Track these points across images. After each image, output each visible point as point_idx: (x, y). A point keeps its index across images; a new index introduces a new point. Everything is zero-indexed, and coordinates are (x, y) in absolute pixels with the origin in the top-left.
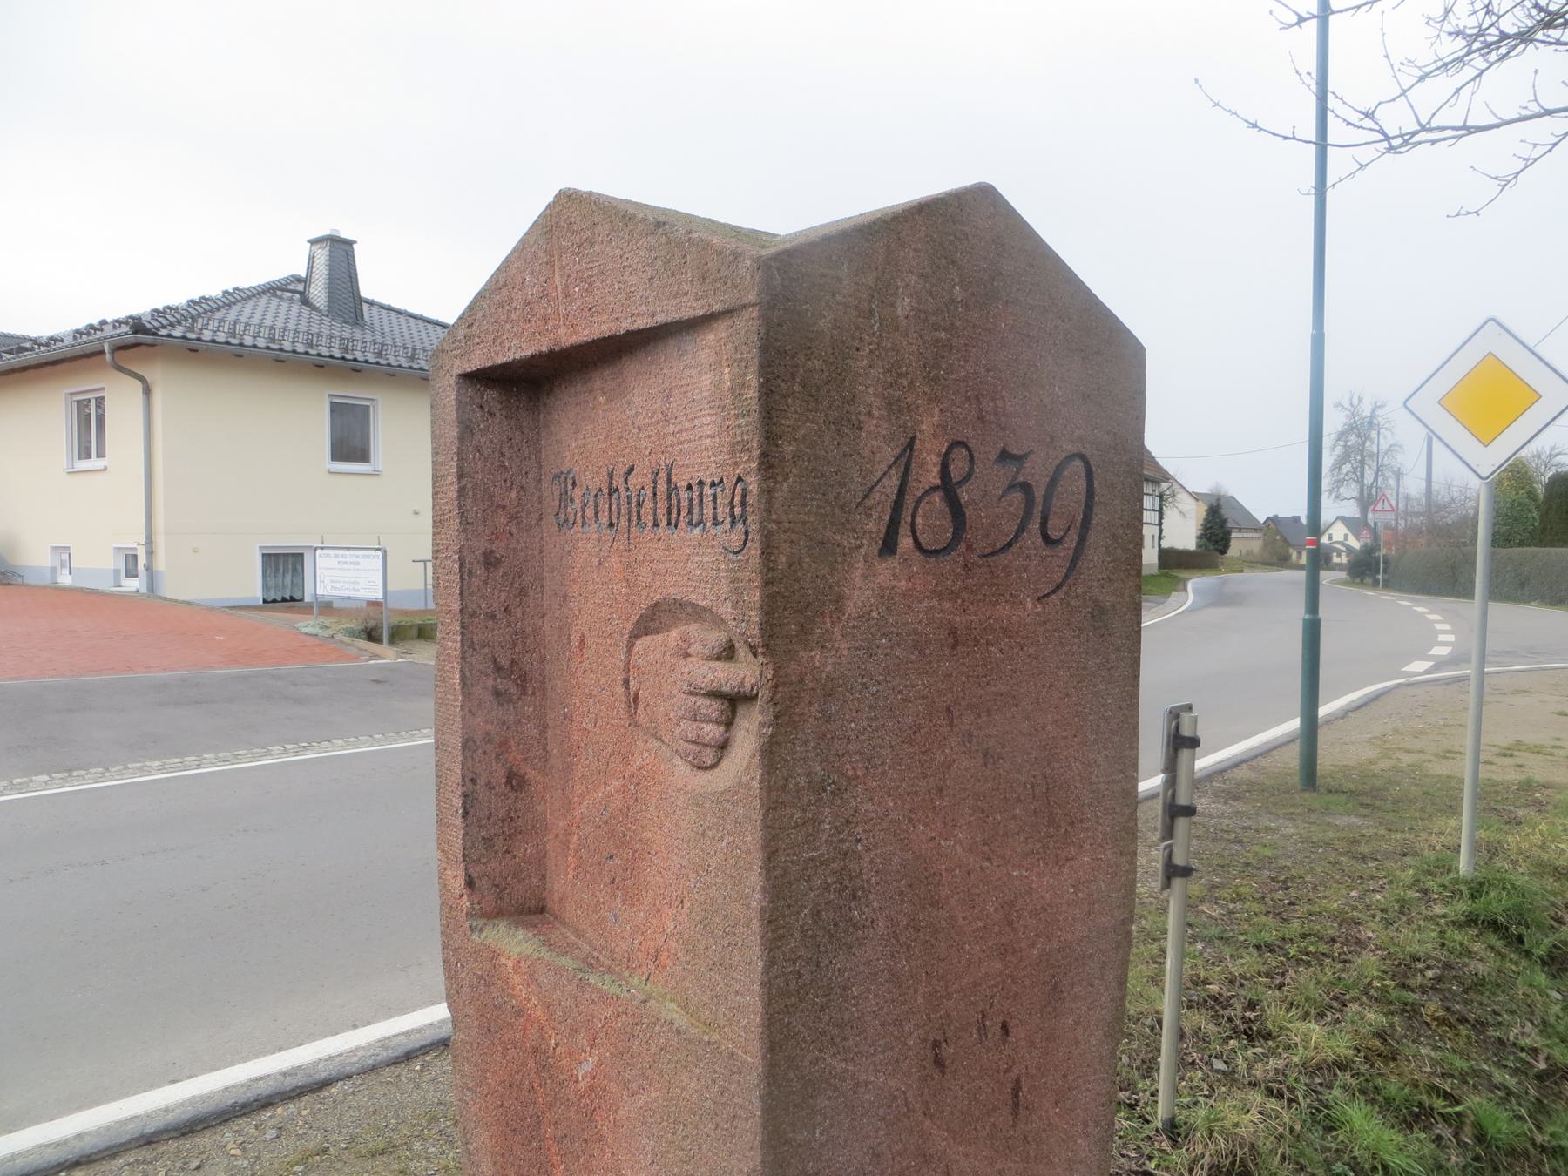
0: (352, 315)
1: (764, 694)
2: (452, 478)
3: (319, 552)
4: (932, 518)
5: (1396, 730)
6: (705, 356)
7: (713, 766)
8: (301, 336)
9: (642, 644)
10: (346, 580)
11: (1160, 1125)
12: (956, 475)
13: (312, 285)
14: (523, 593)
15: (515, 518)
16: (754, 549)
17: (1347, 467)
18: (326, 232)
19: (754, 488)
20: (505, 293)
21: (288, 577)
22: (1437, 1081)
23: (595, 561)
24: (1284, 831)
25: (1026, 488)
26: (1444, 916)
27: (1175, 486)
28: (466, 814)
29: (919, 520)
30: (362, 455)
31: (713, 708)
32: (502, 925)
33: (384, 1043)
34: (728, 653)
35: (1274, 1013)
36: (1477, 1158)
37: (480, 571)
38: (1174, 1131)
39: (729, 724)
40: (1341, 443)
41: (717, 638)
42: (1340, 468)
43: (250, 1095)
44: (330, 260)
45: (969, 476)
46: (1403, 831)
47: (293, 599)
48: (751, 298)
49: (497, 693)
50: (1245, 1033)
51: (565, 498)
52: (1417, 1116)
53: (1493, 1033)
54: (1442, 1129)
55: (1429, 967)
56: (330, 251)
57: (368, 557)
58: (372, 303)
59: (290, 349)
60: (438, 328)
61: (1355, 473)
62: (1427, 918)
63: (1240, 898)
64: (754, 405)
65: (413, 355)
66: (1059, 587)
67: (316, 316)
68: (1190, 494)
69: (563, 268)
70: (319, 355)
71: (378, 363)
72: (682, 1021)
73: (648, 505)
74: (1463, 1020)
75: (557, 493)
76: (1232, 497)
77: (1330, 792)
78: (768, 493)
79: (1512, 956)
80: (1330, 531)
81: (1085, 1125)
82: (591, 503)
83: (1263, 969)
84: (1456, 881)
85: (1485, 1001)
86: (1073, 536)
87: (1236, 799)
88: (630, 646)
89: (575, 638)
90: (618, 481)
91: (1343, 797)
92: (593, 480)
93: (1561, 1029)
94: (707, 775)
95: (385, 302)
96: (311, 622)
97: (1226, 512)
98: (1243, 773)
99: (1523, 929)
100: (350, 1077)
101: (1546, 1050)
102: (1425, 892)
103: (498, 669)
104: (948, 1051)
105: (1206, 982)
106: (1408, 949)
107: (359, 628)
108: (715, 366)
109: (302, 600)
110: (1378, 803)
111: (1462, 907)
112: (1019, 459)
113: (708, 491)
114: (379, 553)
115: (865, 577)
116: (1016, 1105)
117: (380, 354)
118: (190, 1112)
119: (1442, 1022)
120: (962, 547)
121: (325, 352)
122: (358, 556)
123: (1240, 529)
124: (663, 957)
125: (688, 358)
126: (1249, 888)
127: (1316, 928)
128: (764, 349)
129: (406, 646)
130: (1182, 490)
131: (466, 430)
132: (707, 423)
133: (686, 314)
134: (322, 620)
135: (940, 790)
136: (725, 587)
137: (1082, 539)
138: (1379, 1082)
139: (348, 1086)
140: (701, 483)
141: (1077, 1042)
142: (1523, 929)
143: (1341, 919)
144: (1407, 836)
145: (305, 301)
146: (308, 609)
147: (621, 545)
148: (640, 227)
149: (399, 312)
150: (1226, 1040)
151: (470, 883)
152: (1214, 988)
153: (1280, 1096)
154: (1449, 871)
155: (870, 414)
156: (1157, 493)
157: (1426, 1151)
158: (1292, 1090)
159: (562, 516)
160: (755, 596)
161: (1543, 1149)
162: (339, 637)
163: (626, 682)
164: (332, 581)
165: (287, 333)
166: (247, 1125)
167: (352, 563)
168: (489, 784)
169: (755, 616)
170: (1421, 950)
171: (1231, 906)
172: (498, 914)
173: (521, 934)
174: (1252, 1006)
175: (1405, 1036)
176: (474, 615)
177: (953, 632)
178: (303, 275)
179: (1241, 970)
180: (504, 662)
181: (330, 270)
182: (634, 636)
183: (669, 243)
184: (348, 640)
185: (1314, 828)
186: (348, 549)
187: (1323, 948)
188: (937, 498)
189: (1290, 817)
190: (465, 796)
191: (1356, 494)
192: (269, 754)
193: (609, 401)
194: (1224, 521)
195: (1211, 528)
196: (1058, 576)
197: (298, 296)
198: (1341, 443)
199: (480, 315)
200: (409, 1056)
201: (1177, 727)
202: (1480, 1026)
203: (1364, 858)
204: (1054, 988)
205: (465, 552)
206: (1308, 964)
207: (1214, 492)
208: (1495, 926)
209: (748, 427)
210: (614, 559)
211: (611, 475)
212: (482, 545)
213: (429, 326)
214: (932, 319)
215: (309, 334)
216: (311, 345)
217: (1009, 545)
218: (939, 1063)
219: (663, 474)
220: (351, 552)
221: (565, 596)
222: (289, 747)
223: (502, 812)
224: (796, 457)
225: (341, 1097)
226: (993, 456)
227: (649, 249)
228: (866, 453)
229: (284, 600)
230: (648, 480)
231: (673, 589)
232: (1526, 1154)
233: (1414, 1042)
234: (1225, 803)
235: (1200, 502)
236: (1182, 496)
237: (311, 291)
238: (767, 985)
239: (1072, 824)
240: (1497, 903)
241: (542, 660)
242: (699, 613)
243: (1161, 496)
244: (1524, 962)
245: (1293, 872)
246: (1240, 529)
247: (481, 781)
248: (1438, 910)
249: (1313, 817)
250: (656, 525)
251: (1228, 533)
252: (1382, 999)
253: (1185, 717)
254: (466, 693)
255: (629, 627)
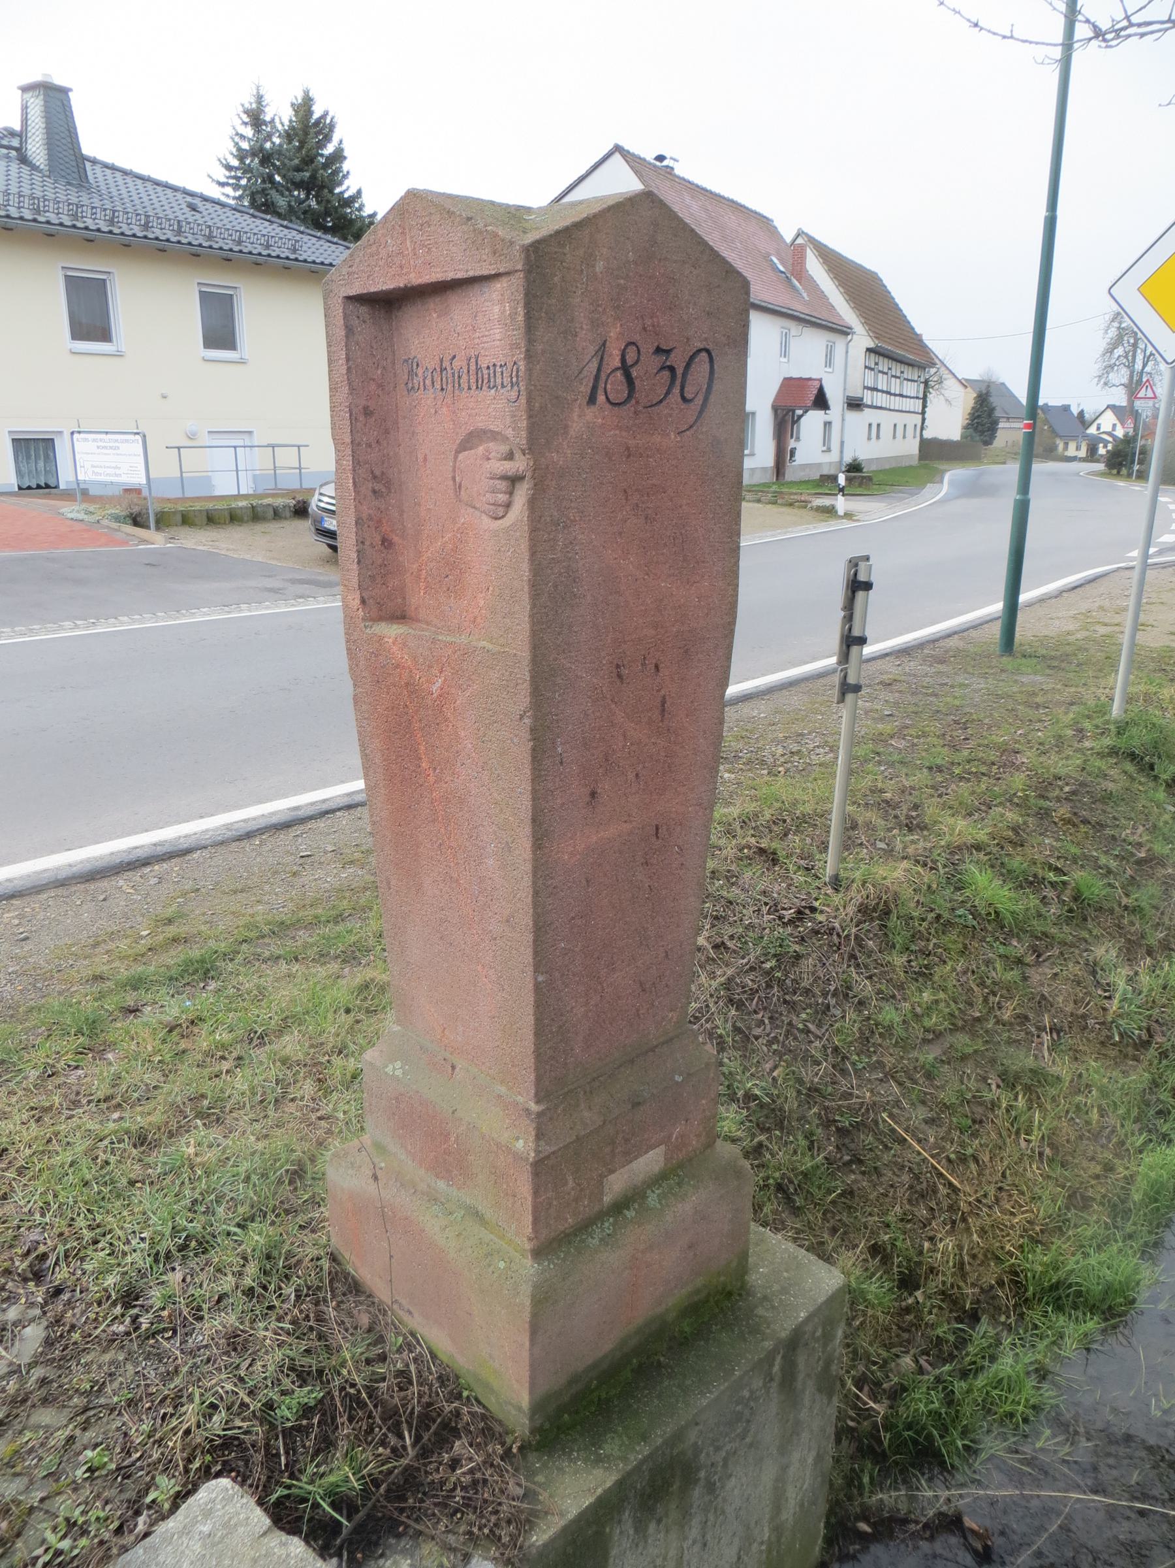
0: (76, 176)
1: (529, 474)
2: (342, 361)
3: (76, 436)
4: (616, 385)
5: (1101, 608)
6: (495, 296)
7: (503, 517)
8: (27, 201)
9: (461, 456)
10: (107, 464)
11: (827, 880)
12: (629, 362)
13: (29, 141)
14: (387, 432)
15: (381, 386)
16: (523, 399)
17: (1119, 351)
18: (37, 77)
19: (522, 368)
20: (374, 248)
21: (41, 464)
22: (1052, 861)
23: (433, 411)
24: (975, 686)
25: (672, 369)
26: (1092, 749)
27: (943, 370)
28: (359, 562)
29: (609, 386)
30: (104, 334)
31: (503, 485)
32: (383, 624)
33: (228, 827)
34: (510, 456)
35: (931, 810)
36: (1070, 911)
37: (362, 418)
38: (837, 883)
39: (511, 493)
40: (1116, 324)
41: (504, 449)
42: (1111, 352)
43: (132, 857)
44: (46, 111)
45: (637, 362)
46: (1077, 686)
47: (47, 486)
48: (520, 267)
49: (374, 492)
50: (907, 825)
51: (412, 374)
52: (1031, 883)
53: (1108, 831)
54: (1050, 893)
55: (1067, 784)
56: (46, 102)
57: (127, 441)
58: (94, 162)
59: (16, 215)
60: (169, 191)
61: (1126, 357)
62: (1077, 750)
63: (925, 735)
64: (522, 324)
65: (147, 223)
66: (691, 427)
67: (37, 177)
68: (960, 381)
69: (412, 237)
70: (48, 222)
71: (110, 232)
72: (489, 646)
73: (465, 377)
74: (1085, 822)
75: (406, 371)
76: (1003, 384)
77: (1025, 656)
78: (529, 370)
79: (1142, 780)
80: (1098, 421)
81: (705, 732)
82: (429, 377)
83: (930, 783)
84: (1107, 722)
85: (1109, 810)
86: (701, 397)
87: (942, 662)
88: (456, 458)
89: (420, 458)
90: (446, 364)
91: (1035, 660)
92: (431, 363)
93: (1166, 830)
94: (500, 522)
95: (108, 160)
96: (76, 508)
97: (994, 400)
98: (953, 643)
99: (1155, 760)
100: (205, 848)
101: (1149, 845)
102: (1081, 731)
103: (375, 477)
104: (625, 672)
105: (882, 791)
106: (1052, 770)
107: (124, 513)
108: (501, 302)
109: (56, 487)
110: (1063, 665)
111: (1107, 741)
112: (668, 352)
113: (498, 369)
114: (137, 437)
115: (580, 416)
116: (663, 710)
117: (111, 222)
118: (88, 867)
119: (1068, 822)
120: (633, 401)
121: (54, 219)
122: (116, 441)
123: (1008, 418)
124: (479, 620)
125: (486, 296)
126: (936, 727)
127: (981, 755)
128: (526, 295)
129: (173, 531)
130: (950, 376)
131: (349, 330)
132: (497, 333)
133: (485, 272)
134: (84, 506)
135: (620, 533)
136: (508, 420)
137: (706, 400)
138: (1006, 859)
139: (205, 853)
140: (494, 365)
141: (700, 685)
142: (1155, 760)
143: (1004, 750)
144: (1080, 690)
145: (24, 160)
146: (68, 495)
147: (449, 400)
148: (458, 219)
149: (125, 173)
150: (890, 830)
151: (363, 601)
152: (888, 795)
153: (925, 865)
154: (1105, 714)
155: (581, 328)
156: (922, 379)
157: (1032, 904)
158: (935, 862)
159: (410, 385)
160: (524, 424)
161: (1126, 908)
162: (105, 522)
163: (454, 479)
164: (93, 466)
165: (11, 197)
166: (136, 876)
167: (111, 448)
168: (371, 545)
169: (524, 434)
170: (1062, 772)
171: (916, 741)
172: (380, 619)
173: (395, 626)
174: (916, 807)
175: (1035, 831)
176: (359, 444)
177: (628, 449)
178: (17, 127)
179: (912, 784)
180: (378, 473)
181: (47, 123)
182: (458, 452)
183: (474, 230)
184: (115, 525)
185: (1001, 684)
186: (107, 433)
187: (984, 769)
188: (619, 374)
189: (985, 676)
190: (358, 551)
191: (1125, 380)
192: (62, 628)
193: (439, 317)
194: (992, 410)
195: (979, 417)
196: (691, 420)
197: (14, 153)
198: (1116, 324)
199: (357, 260)
200: (249, 835)
201: (856, 574)
202: (1101, 826)
203: (1038, 706)
204: (686, 652)
205: (353, 407)
206: (968, 780)
207: (985, 378)
208: (1132, 756)
209: (518, 335)
210: (444, 409)
211: (442, 361)
212: (363, 402)
213: (159, 189)
214: (615, 273)
215: (20, 196)
216: (38, 212)
217: (661, 401)
218: (619, 676)
219: (473, 360)
220: (109, 436)
221: (413, 433)
222: (78, 622)
223: (380, 561)
224: (543, 352)
225: (201, 860)
226: (651, 351)
227: (464, 233)
228: (580, 349)
229: (39, 487)
230: (464, 364)
231: (480, 423)
232: (1112, 911)
233: (1041, 834)
234: (931, 666)
235: (969, 389)
236: (950, 383)
237: (29, 147)
238: (532, 616)
239: (697, 562)
240: (1138, 738)
241: (400, 472)
242: (494, 436)
243: (926, 383)
244: (1152, 784)
245: (974, 717)
246: (1008, 418)
247: (367, 543)
248: (1087, 744)
249: (1004, 676)
250: (469, 388)
251: (995, 423)
252: (1022, 805)
253: (862, 565)
254: (357, 492)
255: (455, 447)
